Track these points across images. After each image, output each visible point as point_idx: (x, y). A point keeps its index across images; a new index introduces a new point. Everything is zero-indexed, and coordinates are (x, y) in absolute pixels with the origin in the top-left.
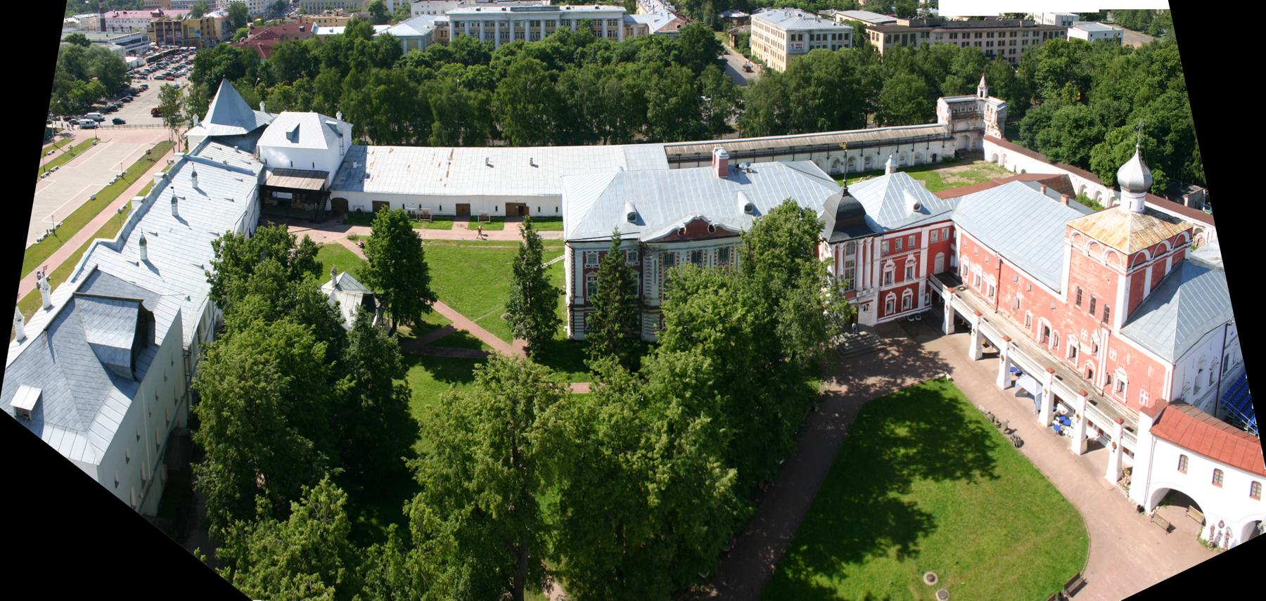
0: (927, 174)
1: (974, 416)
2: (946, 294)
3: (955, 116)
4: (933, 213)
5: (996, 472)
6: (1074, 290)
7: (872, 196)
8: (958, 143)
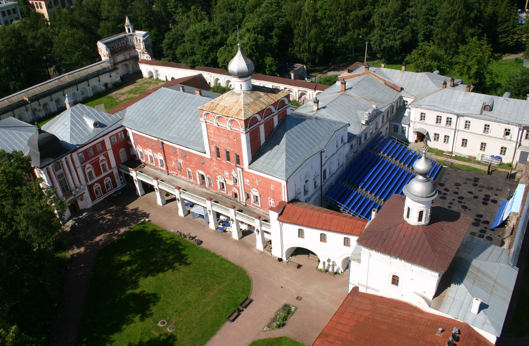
0: (104, 99)
1: (168, 236)
2: (133, 174)
3: (113, 51)
4: (108, 126)
5: (189, 261)
6: (214, 149)
7: (61, 128)
8: (121, 71)
